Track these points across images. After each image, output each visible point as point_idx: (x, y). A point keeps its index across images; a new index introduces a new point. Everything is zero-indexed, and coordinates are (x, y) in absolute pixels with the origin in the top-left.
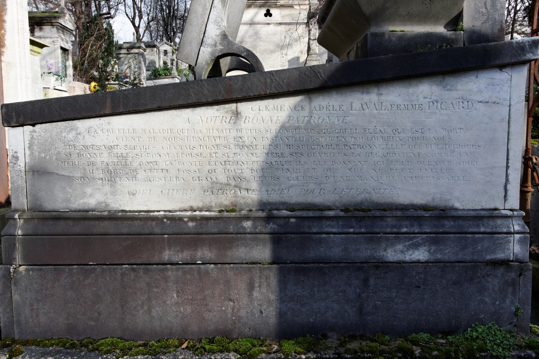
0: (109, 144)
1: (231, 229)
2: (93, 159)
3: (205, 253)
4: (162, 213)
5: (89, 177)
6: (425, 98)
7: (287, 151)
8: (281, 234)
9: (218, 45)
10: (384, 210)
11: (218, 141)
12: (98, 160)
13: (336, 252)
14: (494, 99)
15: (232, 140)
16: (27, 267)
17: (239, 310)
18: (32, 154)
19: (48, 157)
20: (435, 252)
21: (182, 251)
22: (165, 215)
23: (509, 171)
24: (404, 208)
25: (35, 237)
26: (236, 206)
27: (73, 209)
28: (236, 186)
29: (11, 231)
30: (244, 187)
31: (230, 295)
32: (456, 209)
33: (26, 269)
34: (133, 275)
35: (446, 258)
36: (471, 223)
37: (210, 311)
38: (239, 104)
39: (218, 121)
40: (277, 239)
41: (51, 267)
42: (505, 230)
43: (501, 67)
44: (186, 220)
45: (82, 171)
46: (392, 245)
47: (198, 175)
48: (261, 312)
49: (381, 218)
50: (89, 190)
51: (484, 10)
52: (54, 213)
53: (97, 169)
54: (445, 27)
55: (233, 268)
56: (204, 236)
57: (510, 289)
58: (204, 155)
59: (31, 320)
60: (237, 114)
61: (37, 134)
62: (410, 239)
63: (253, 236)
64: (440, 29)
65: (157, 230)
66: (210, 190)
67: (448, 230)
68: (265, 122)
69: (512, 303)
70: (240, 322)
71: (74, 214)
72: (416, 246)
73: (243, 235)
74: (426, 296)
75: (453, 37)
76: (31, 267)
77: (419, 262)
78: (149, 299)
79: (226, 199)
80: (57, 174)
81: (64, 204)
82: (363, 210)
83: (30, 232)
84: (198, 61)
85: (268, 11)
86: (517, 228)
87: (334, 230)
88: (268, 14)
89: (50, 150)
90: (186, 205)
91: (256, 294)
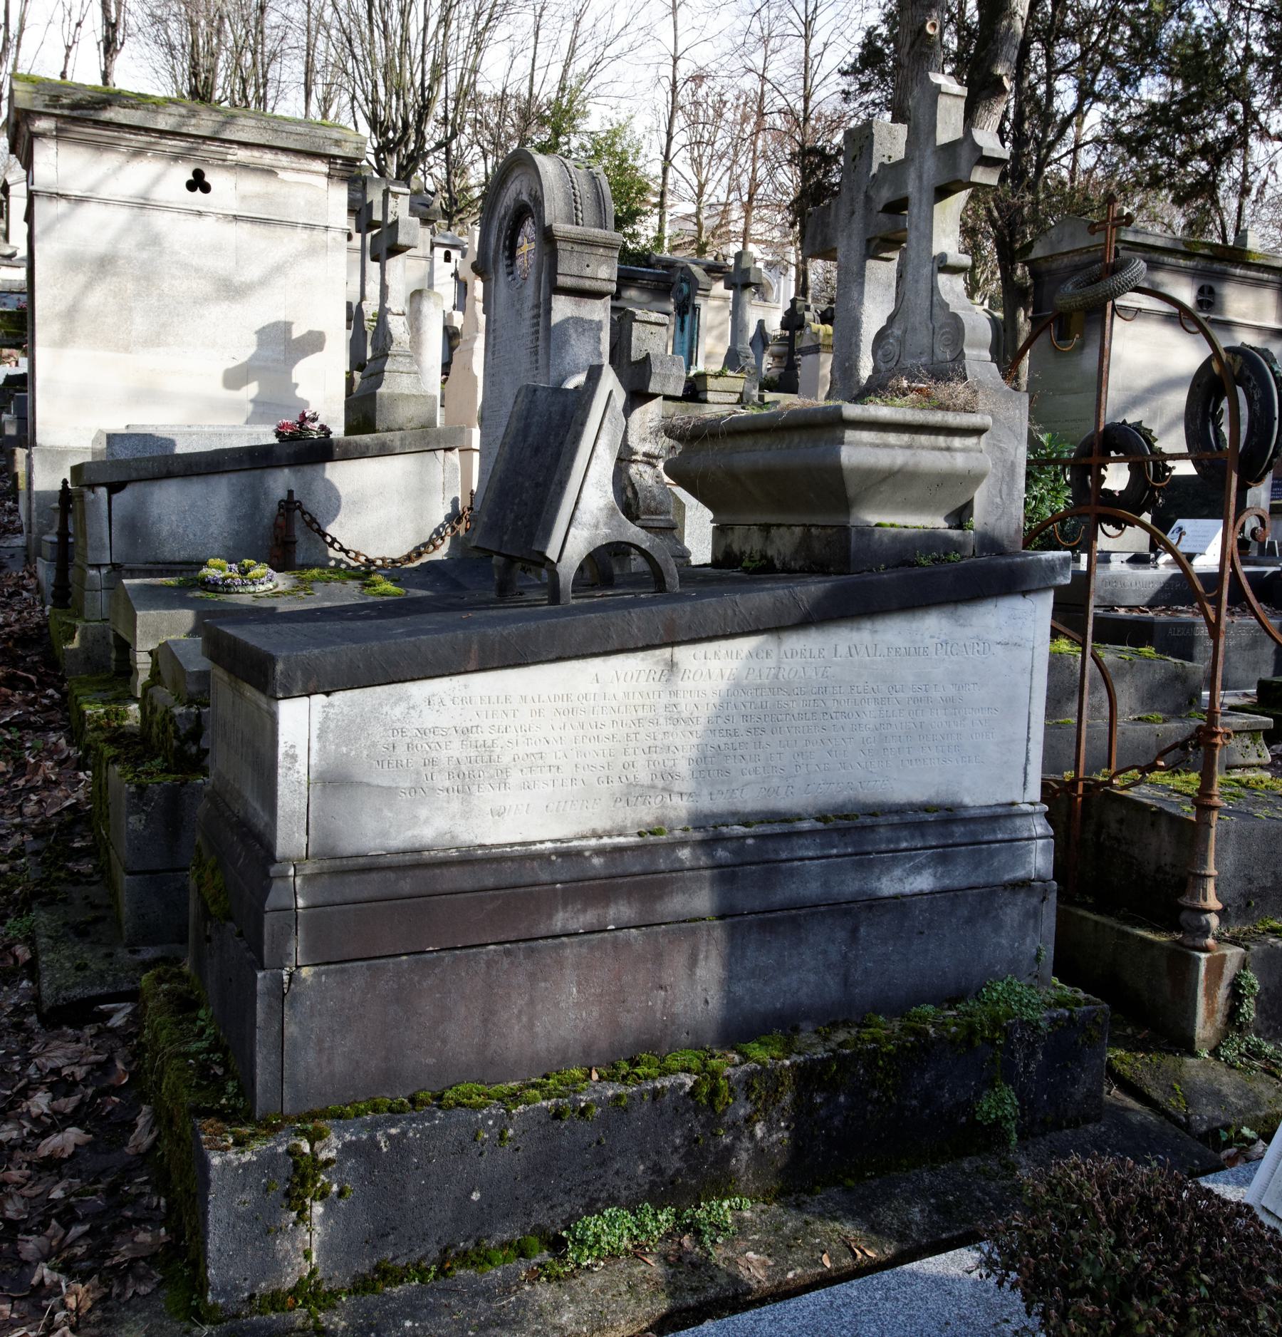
0: (464, 725)
1: (662, 864)
2: (434, 754)
3: (622, 911)
4: (549, 845)
5: (424, 786)
6: (932, 637)
7: (742, 726)
8: (735, 866)
9: (601, 525)
10: (874, 815)
11: (640, 714)
12: (443, 755)
13: (813, 889)
14: (1016, 640)
15: (661, 711)
16: (316, 968)
17: (673, 1003)
18: (323, 749)
19: (353, 753)
20: (942, 876)
21: (584, 911)
22: (555, 848)
23: (1030, 745)
24: (899, 809)
25: (328, 909)
26: (663, 824)
27: (393, 850)
28: (664, 789)
29: (285, 901)
30: (676, 789)
31: (660, 978)
32: (966, 807)
33: (315, 973)
34: (506, 962)
35: (956, 884)
36: (984, 826)
37: (628, 1011)
38: (676, 649)
39: (643, 677)
40: (726, 876)
41: (360, 963)
42: (1026, 835)
43: (1024, 593)
44: (587, 854)
45: (414, 776)
46: (889, 870)
47: (607, 772)
48: (707, 1002)
49: (872, 828)
50: (423, 813)
51: (998, 500)
52: (361, 860)
53: (439, 772)
54: (946, 519)
55: (667, 931)
56: (620, 881)
57: (1031, 922)
58: (618, 737)
59: (317, 1071)
60: (672, 665)
61: (336, 710)
62: (911, 858)
63: (696, 872)
64: (937, 522)
65: (545, 877)
66: (624, 799)
67: (958, 840)
68: (713, 677)
69: (1034, 942)
70: (673, 1023)
71: (400, 857)
72: (917, 870)
73: (680, 874)
74: (931, 946)
75: (961, 538)
76: (323, 968)
77: (921, 894)
78: (532, 1002)
79: (646, 813)
80: (368, 785)
81: (378, 841)
82: (846, 817)
83: (320, 900)
84: (565, 553)
85: (198, 174)
86: (1039, 830)
87: (811, 854)
88: (198, 183)
89: (357, 739)
90: (585, 828)
91: (700, 972)
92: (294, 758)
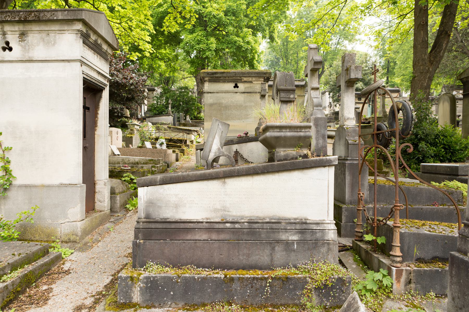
50: (167, 211)
62: (291, 232)
86: (332, 228)
88: (236, 86)
90: (204, 217)
92: (141, 199)
